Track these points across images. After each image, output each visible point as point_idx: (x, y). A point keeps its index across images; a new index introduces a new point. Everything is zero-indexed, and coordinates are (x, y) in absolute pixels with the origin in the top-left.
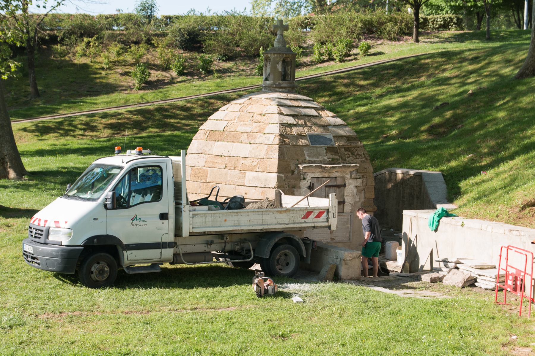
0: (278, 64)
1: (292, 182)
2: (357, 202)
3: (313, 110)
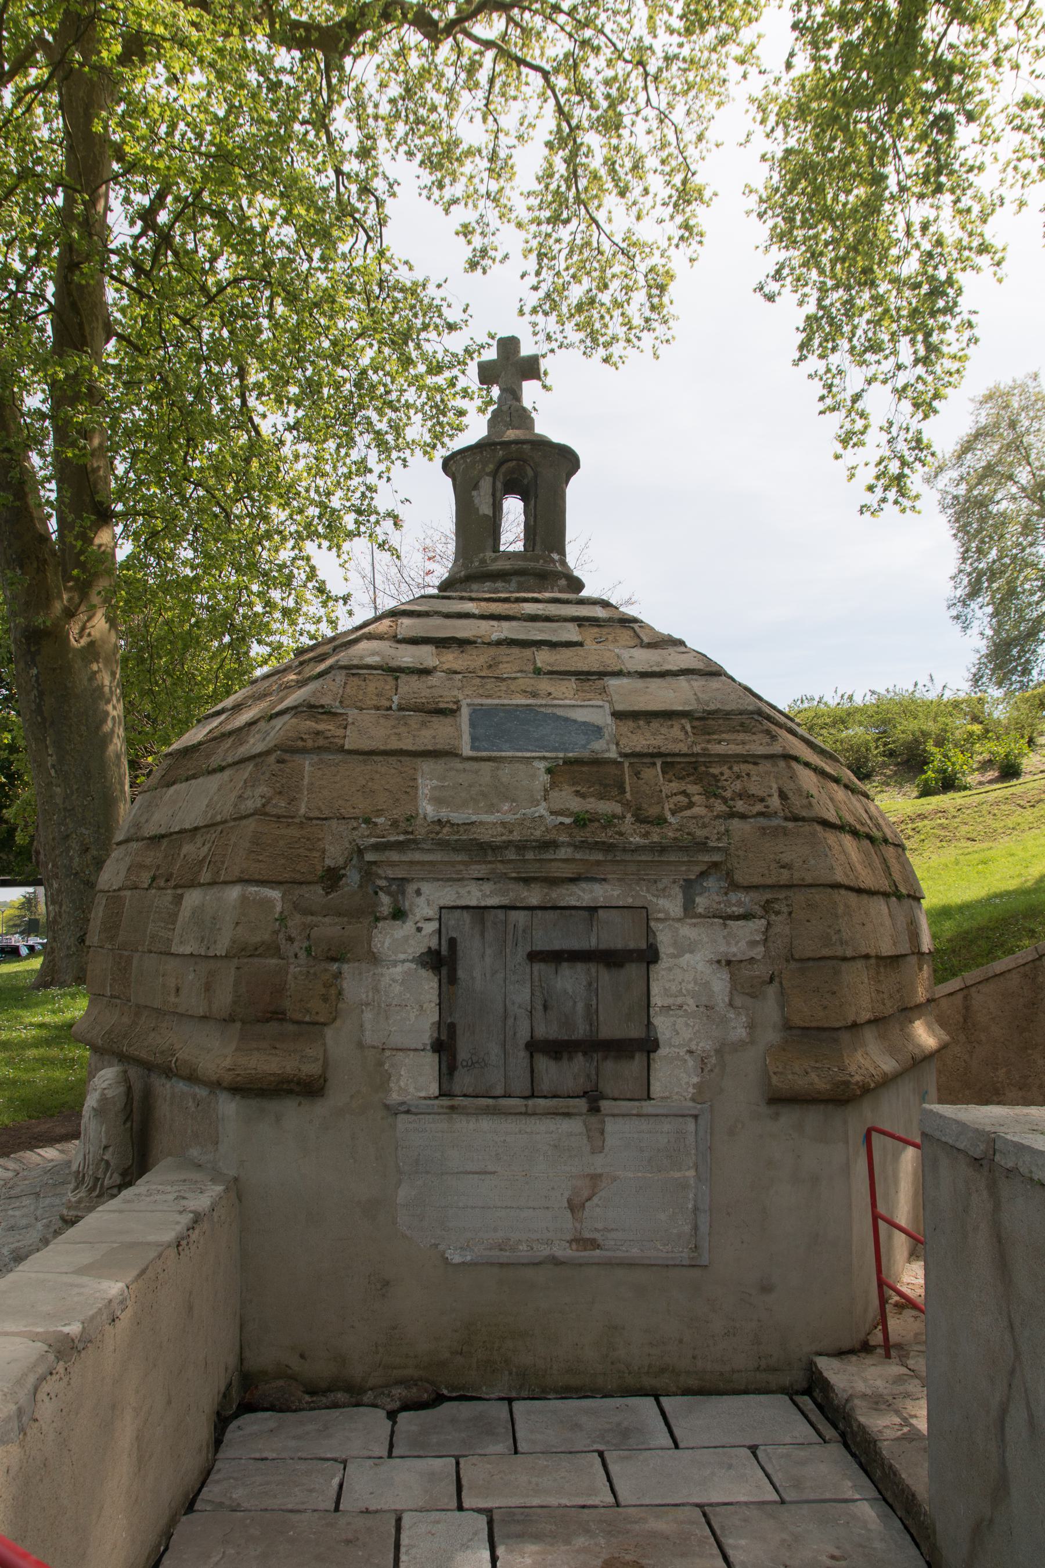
0: (476, 487)
1: (329, 929)
2: (739, 1046)
3: (572, 626)
